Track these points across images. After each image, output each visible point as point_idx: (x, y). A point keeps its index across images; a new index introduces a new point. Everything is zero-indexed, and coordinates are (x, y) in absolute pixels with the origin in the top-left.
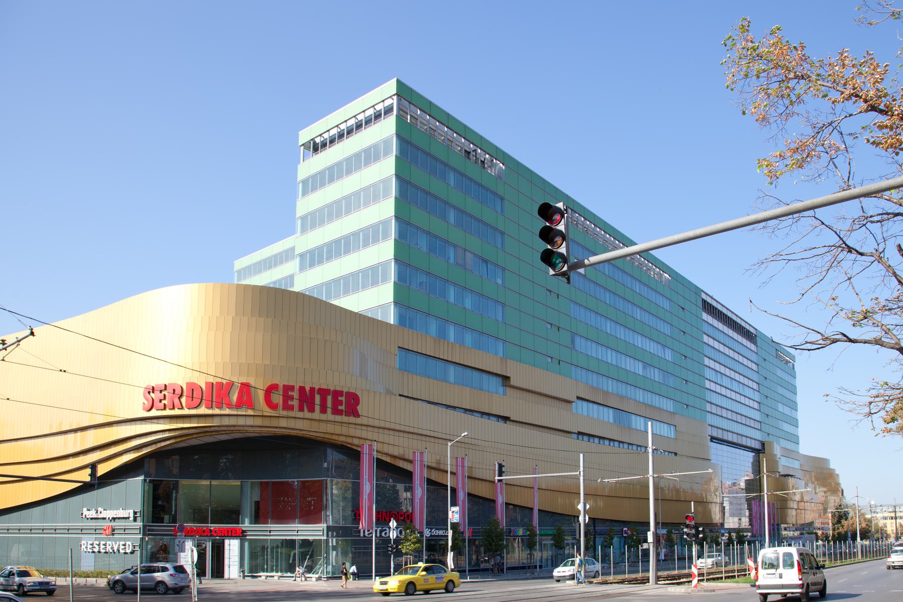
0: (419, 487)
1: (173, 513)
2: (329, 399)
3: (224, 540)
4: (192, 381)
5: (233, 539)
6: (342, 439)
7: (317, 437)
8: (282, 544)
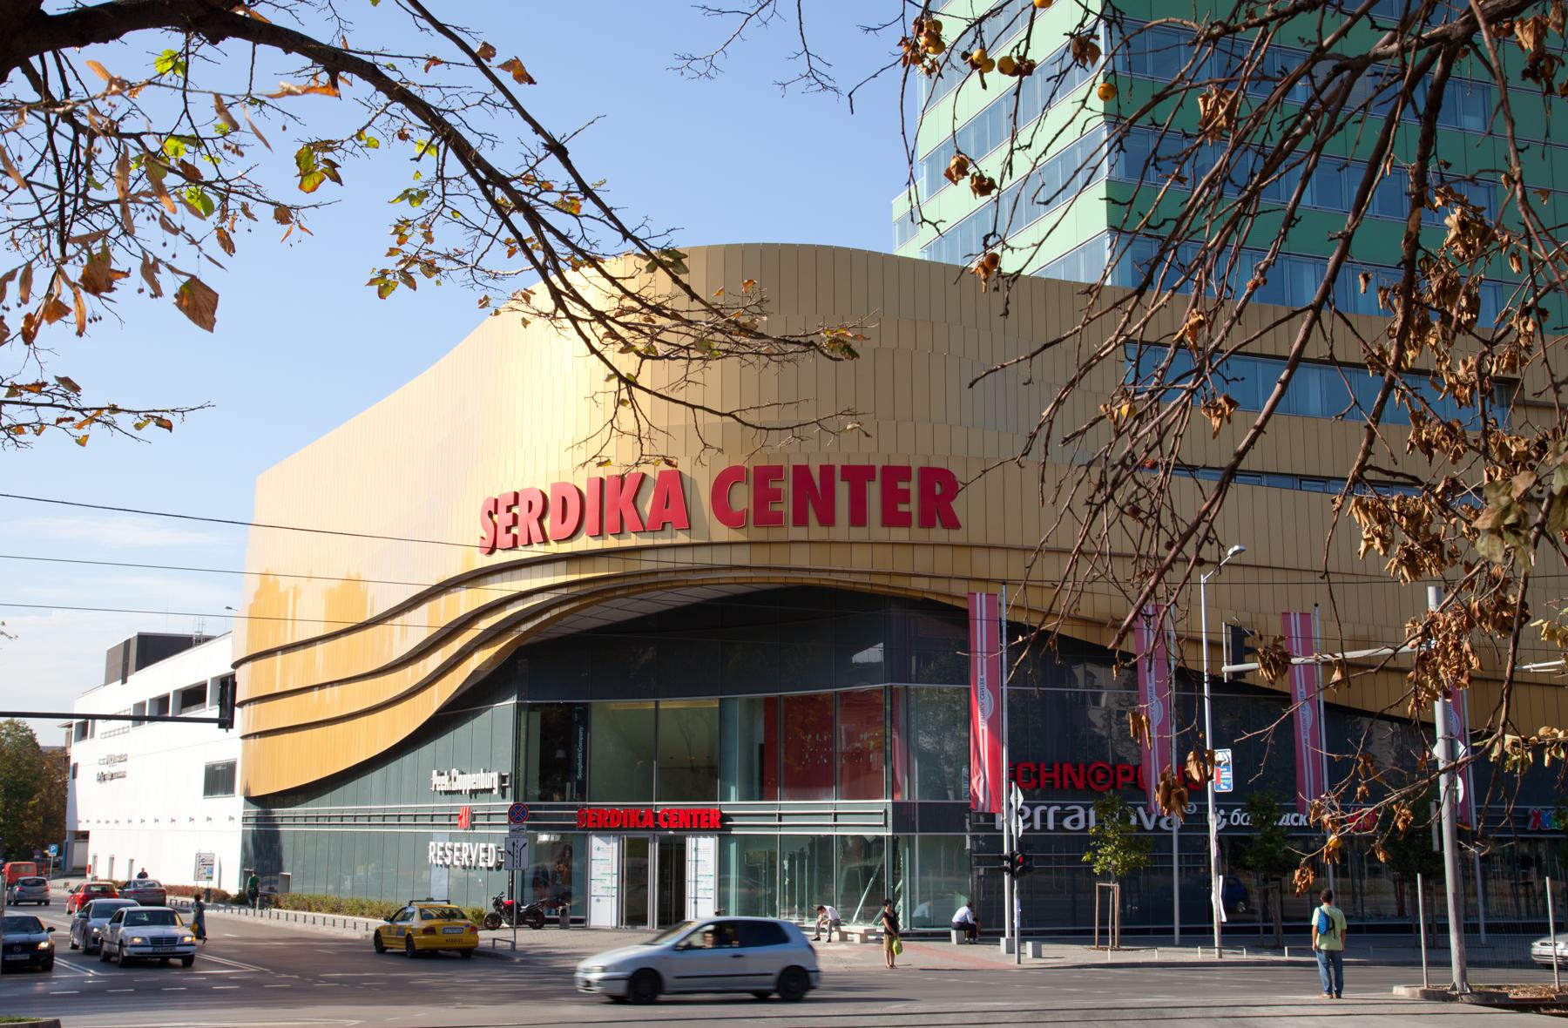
0: (986, 691)
1: (579, 776)
2: (874, 491)
3: (684, 838)
4: (563, 480)
5: (705, 836)
6: (921, 584)
7: (854, 583)
8: (811, 846)
